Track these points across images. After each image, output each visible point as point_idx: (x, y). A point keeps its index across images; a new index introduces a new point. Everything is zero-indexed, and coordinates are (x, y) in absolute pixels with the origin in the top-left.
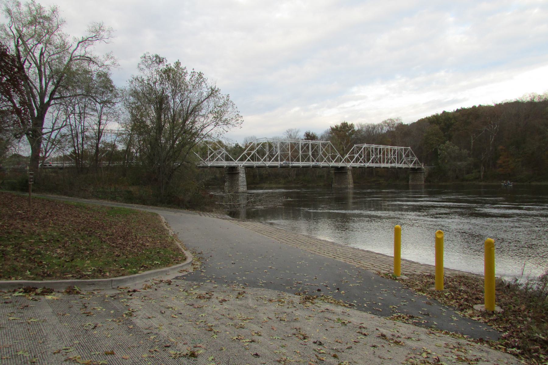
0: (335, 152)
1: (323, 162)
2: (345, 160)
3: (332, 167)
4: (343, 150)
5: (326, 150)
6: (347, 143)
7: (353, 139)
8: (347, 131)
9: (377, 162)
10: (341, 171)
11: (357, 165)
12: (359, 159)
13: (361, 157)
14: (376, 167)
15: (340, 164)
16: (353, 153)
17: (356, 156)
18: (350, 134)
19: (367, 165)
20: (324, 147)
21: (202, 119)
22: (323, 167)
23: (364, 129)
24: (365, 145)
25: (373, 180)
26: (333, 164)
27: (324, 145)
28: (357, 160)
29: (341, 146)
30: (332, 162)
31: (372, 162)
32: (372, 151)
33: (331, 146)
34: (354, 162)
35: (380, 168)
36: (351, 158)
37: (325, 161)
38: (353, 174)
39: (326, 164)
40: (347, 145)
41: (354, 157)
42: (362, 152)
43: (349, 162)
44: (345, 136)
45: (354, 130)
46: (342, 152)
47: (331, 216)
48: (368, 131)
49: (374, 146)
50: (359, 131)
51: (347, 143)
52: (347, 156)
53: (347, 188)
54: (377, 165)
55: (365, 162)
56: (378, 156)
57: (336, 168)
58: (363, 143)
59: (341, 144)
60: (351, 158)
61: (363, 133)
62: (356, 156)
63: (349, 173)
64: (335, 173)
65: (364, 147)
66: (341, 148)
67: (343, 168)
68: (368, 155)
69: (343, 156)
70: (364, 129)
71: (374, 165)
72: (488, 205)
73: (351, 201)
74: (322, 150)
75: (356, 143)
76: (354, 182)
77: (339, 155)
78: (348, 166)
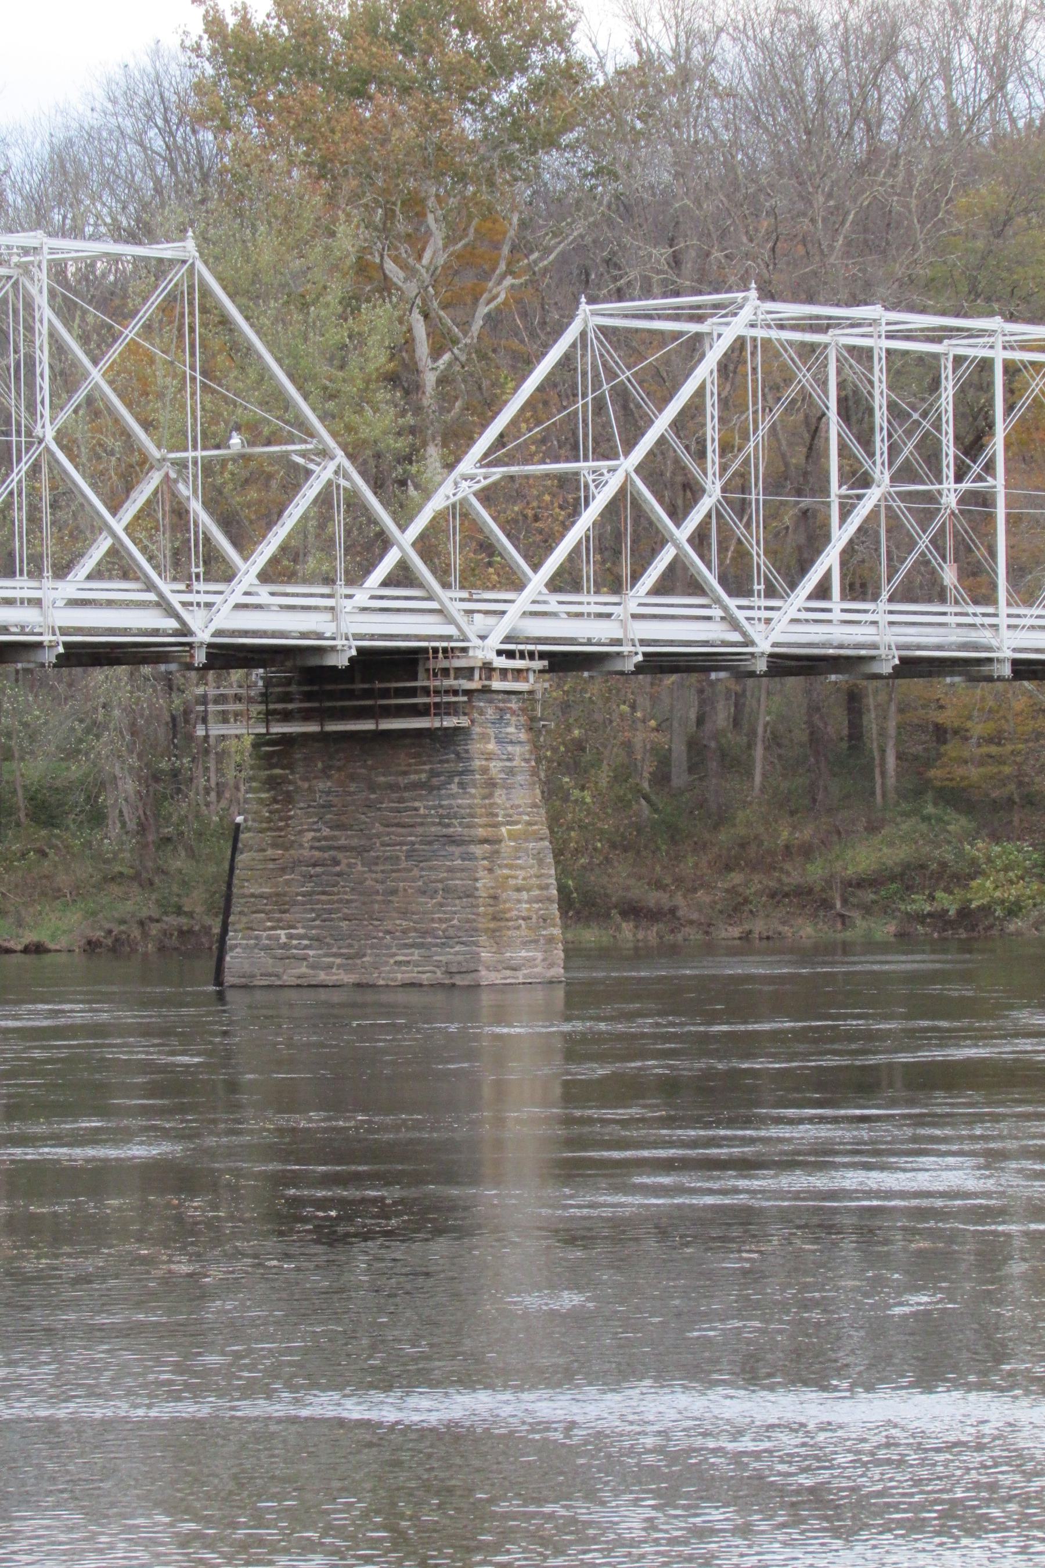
0: (275, 422)
1: (73, 586)
2: (428, 545)
3: (227, 656)
4: (402, 378)
5: (136, 385)
6: (470, 267)
7: (561, 208)
8: (466, 82)
9: (922, 588)
10: (362, 712)
11: (629, 622)
12: (650, 541)
13: (681, 494)
14: (911, 667)
15: (348, 619)
16: (558, 428)
17: (609, 478)
18: (521, 138)
19: (782, 623)
20: (96, 341)
21: (737, 1359)
22: (86, 655)
23: (732, 62)
24: (746, 317)
25: (864, 857)
26: (243, 605)
27: (96, 301)
28: (621, 549)
29: (378, 315)
30: (219, 570)
31: (859, 586)
32: (854, 408)
33: (208, 306)
34: (565, 581)
35: (971, 668)
36: (532, 514)
37: (116, 565)
38: (563, 764)
39: (126, 616)
40: (461, 302)
41: (570, 495)
42: (688, 421)
43: (485, 571)
44: (440, 159)
45: (572, 74)
46: (380, 421)
47: (75, 1161)
48: (782, 80)
49: (877, 326)
50: (654, 88)
51: (470, 267)
52: (459, 483)
53: (458, 989)
54: (938, 630)
55: (737, 583)
56: (950, 493)
57: (298, 678)
58: (700, 268)
59: (368, 279)
60: (532, 514)
61: (715, 123)
62: (609, 478)
63: (501, 752)
64: (276, 753)
65: (723, 334)
66: (378, 358)
67: (388, 670)
68: (798, 471)
69: (394, 476)
70: (732, 62)
71: (881, 629)
72: (969, 1042)
73: (517, 1201)
74: (66, 377)
75: (594, 273)
76: (578, 904)
77: (331, 469)
78: (485, 651)
